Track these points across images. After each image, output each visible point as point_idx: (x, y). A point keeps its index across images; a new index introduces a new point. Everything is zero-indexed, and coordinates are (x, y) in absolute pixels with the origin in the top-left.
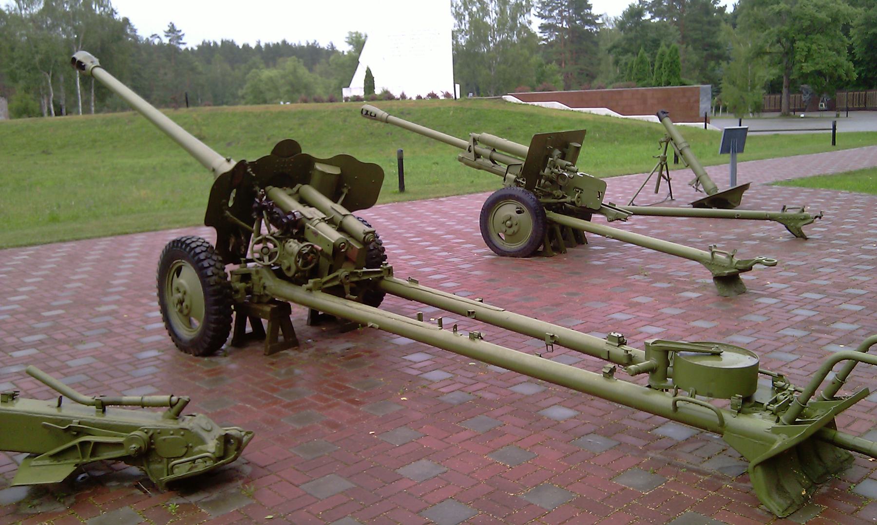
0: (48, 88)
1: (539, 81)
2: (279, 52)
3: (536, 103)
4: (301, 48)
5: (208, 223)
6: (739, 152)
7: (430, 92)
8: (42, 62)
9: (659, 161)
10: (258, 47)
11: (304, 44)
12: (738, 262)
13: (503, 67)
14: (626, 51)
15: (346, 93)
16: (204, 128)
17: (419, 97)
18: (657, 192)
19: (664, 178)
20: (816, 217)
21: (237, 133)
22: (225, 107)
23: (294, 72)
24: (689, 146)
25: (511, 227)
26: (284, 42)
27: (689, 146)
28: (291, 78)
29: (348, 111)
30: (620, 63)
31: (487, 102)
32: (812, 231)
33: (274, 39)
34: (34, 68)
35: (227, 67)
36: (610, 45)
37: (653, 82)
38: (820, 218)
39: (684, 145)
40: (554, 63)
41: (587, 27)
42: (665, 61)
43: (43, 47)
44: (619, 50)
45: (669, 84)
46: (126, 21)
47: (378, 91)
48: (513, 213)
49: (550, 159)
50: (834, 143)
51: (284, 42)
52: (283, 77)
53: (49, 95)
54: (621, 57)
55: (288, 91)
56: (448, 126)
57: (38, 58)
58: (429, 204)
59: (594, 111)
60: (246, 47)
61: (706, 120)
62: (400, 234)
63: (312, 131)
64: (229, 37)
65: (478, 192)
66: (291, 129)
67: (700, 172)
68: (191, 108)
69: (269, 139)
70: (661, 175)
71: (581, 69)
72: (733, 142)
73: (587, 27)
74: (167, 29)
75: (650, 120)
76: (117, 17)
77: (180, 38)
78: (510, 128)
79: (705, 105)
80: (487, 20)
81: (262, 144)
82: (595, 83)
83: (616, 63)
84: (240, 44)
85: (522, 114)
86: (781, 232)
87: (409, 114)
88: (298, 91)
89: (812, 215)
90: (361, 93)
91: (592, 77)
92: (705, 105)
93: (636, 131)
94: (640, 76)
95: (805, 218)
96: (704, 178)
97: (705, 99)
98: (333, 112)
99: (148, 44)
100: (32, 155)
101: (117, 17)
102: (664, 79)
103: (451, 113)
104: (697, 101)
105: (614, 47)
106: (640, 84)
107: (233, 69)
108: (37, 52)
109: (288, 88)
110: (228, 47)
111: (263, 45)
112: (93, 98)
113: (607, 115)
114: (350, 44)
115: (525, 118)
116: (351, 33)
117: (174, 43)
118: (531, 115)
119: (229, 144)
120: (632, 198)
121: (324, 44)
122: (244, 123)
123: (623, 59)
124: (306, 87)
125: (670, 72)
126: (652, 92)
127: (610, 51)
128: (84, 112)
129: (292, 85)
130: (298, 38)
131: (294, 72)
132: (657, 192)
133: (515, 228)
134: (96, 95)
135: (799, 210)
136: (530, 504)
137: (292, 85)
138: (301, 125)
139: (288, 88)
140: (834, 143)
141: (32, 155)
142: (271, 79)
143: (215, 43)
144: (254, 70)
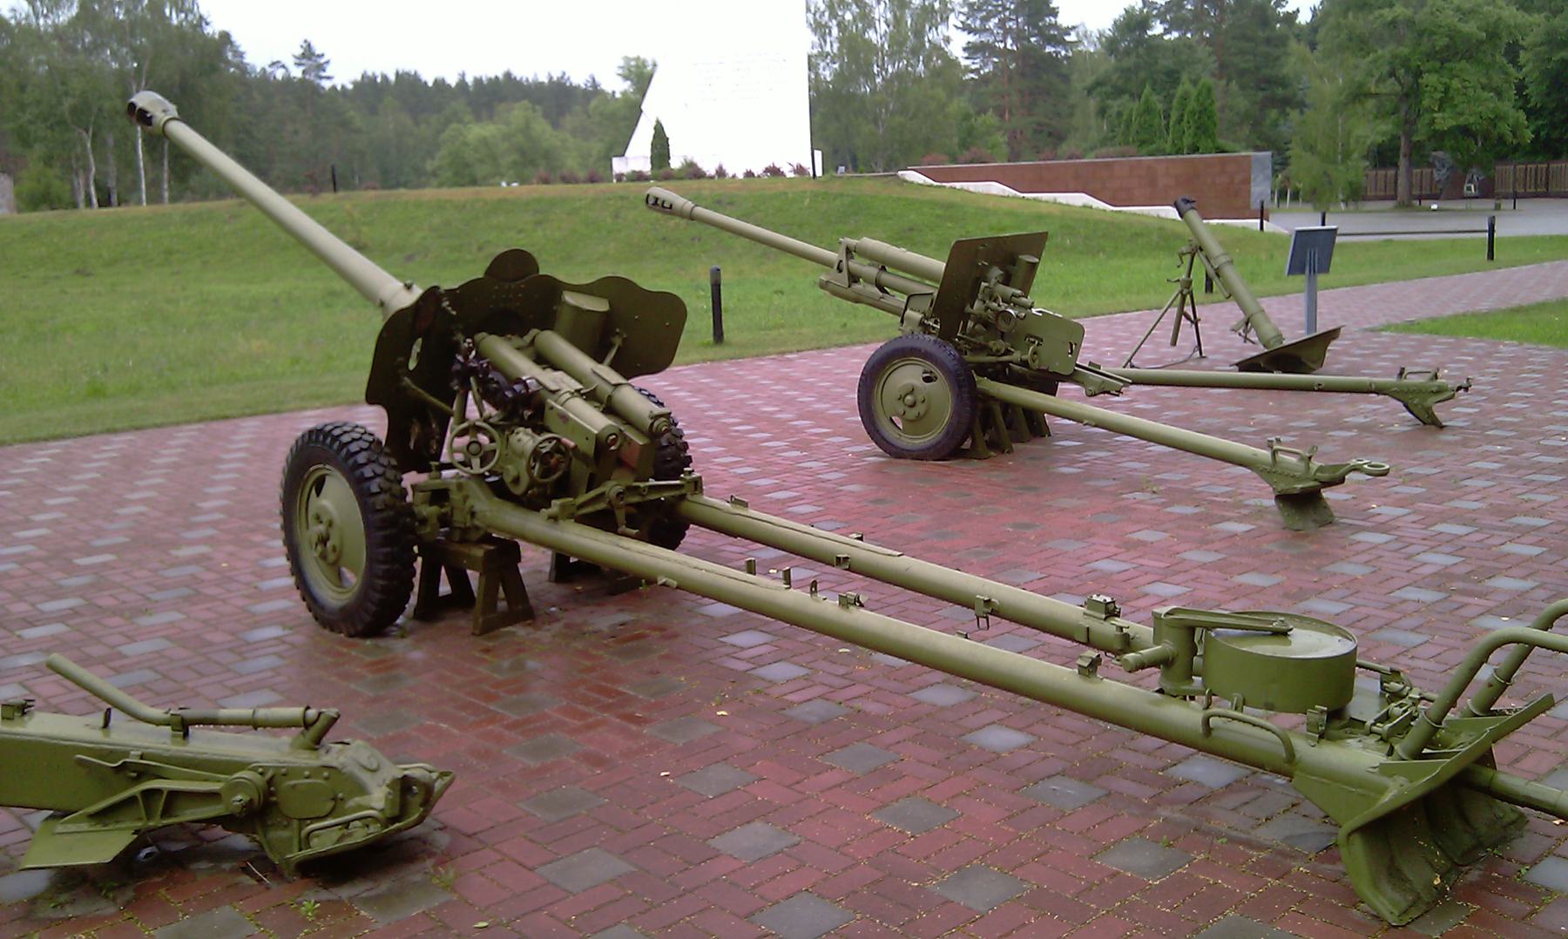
0: (86, 157)
1: (964, 145)
2: (498, 93)
3: (958, 185)
4: (539, 86)
5: (371, 399)
6: (1321, 271)
7: (768, 164)
8: (74, 111)
9: (1178, 287)
10: (462, 83)
11: (544, 79)
12: (1320, 469)
13: (899, 119)
14: (1119, 92)
15: (619, 166)
16: (365, 229)
17: (749, 174)
18: (1174, 343)
19: (1188, 318)
20: (1459, 388)
21: (424, 238)
22: (402, 191)
23: (526, 129)
24: (1231, 262)
25: (913, 406)
26: (508, 75)
27: (1231, 262)
28: (520, 139)
29: (622, 198)
30: (1109, 112)
31: (871, 183)
32: (1452, 413)
33: (491, 69)
34: (61, 122)
35: (407, 120)
36: (1090, 80)
37: (1168, 147)
38: (1466, 389)
39: (1223, 259)
40: (990, 112)
41: (1049, 49)
42: (1189, 108)
43: (76, 84)
44: (1108, 89)
45: (1195, 150)
46: (225, 37)
47: (675, 163)
48: (918, 381)
49: (984, 284)
50: (1491, 256)
51: (508, 75)
52: (506, 137)
53: (87, 170)
54: (1110, 102)
55: (514, 163)
56: (800, 226)
57: (68, 103)
58: (767, 364)
59: (1063, 198)
60: (440, 84)
61: (1262, 215)
62: (715, 418)
63: (557, 234)
64: (409, 67)
65: (854, 344)
66: (520, 231)
67: (1252, 308)
68: (341, 194)
69: (480, 249)
70: (1182, 313)
71: (1039, 124)
72: (1311, 255)
73: (1049, 49)
74: (299, 52)
75: (1163, 215)
76: (208, 30)
77: (321, 67)
78: (911, 229)
79: (1261, 188)
80: (871, 35)
81: (468, 257)
82: (1064, 148)
83: (1102, 112)
84: (429, 78)
85: (934, 204)
86: (1396, 416)
87: (731, 204)
88: (533, 163)
89: (1452, 384)
90: (645, 166)
91: (1058, 137)
92: (1261, 188)
93: (1137, 235)
94: (1143, 136)
95: (1440, 391)
96: (1258, 318)
97: (1261, 177)
98: (595, 200)
99: (265, 79)
100: (57, 278)
101: (208, 30)
102: (1187, 141)
103: (807, 201)
104: (1247, 182)
105: (1098, 84)
106: (1145, 149)
107: (417, 124)
108: (66, 94)
109: (515, 157)
110: (408, 84)
111: (469, 80)
112: (166, 175)
113: (1085, 206)
114: (626, 78)
115: (938, 212)
116: (627, 59)
117: (311, 77)
118: (950, 206)
119: (409, 258)
120: (1129, 354)
121: (579, 79)
122: (436, 220)
123: (1114, 105)
124: (548, 155)
125: (1198, 128)
126: (1166, 165)
127: (1090, 91)
128: (150, 201)
129: (523, 153)
130: (533, 68)
131: (526, 129)
132: (1174, 343)
133: (920, 408)
134: (172, 170)
135: (1429, 376)
136: (947, 902)
137: (523, 153)
138: (538, 223)
139: (515, 157)
140: (1491, 256)
141: (57, 278)
142: (484, 142)
143: (385, 78)
144: (454, 126)
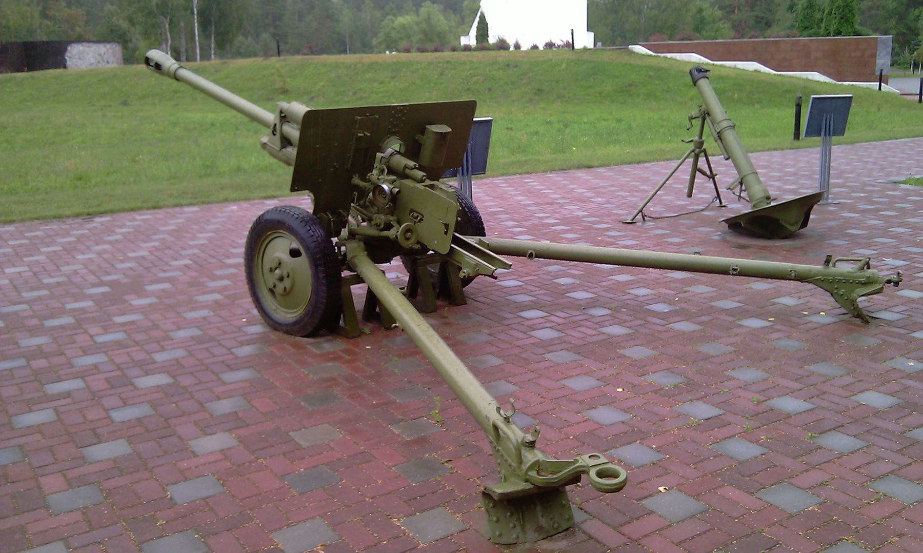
0: (166, 35)
1: (698, 29)
3: (669, 55)
5: (297, 185)
6: (835, 134)
9: (691, 146)
12: (537, 466)
13: (655, 12)
15: (464, 41)
16: (288, 80)
17: (535, 47)
18: (690, 195)
19: (704, 173)
20: (889, 282)
21: (323, 86)
22: (325, 56)
23: (428, 19)
24: (733, 127)
25: (281, 279)
27: (733, 127)
28: (424, 25)
29: (448, 62)
30: (795, 8)
31: (609, 53)
32: (886, 308)
34: (150, 13)
37: (822, 31)
38: (897, 284)
39: (725, 124)
42: (836, 4)
45: (839, 33)
47: (492, 40)
48: (285, 256)
49: (379, 155)
52: (417, 24)
53: (167, 41)
55: (420, 40)
56: (557, 82)
59: (741, 65)
61: (881, 79)
66: (381, 83)
67: (746, 169)
68: (282, 58)
69: (355, 94)
70: (696, 169)
71: (757, 17)
72: (826, 119)
75: (810, 77)
78: (630, 85)
79: (883, 61)
81: (346, 99)
85: (649, 68)
86: (823, 309)
87: (516, 66)
89: (885, 274)
91: (768, 25)
92: (883, 61)
93: (788, 91)
94: (806, 24)
95: (869, 282)
96: (750, 179)
97: (884, 53)
98: (430, 63)
100: (110, 106)
102: (833, 28)
103: (564, 65)
104: (874, 56)
106: (806, 33)
109: (421, 36)
112: (213, 46)
113: (756, 71)
115: (651, 73)
118: (659, 70)
120: (642, 205)
122: (333, 75)
124: (441, 36)
125: (842, 18)
126: (816, 43)
128: (202, 58)
131: (428, 19)
132: (690, 195)
133: (287, 283)
134: (216, 42)
135: (859, 265)
138: (393, 78)
139: (421, 36)
141: (110, 106)
142: (403, 27)
144: (390, 17)
